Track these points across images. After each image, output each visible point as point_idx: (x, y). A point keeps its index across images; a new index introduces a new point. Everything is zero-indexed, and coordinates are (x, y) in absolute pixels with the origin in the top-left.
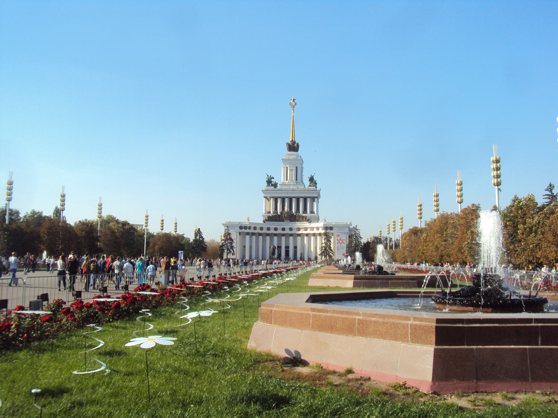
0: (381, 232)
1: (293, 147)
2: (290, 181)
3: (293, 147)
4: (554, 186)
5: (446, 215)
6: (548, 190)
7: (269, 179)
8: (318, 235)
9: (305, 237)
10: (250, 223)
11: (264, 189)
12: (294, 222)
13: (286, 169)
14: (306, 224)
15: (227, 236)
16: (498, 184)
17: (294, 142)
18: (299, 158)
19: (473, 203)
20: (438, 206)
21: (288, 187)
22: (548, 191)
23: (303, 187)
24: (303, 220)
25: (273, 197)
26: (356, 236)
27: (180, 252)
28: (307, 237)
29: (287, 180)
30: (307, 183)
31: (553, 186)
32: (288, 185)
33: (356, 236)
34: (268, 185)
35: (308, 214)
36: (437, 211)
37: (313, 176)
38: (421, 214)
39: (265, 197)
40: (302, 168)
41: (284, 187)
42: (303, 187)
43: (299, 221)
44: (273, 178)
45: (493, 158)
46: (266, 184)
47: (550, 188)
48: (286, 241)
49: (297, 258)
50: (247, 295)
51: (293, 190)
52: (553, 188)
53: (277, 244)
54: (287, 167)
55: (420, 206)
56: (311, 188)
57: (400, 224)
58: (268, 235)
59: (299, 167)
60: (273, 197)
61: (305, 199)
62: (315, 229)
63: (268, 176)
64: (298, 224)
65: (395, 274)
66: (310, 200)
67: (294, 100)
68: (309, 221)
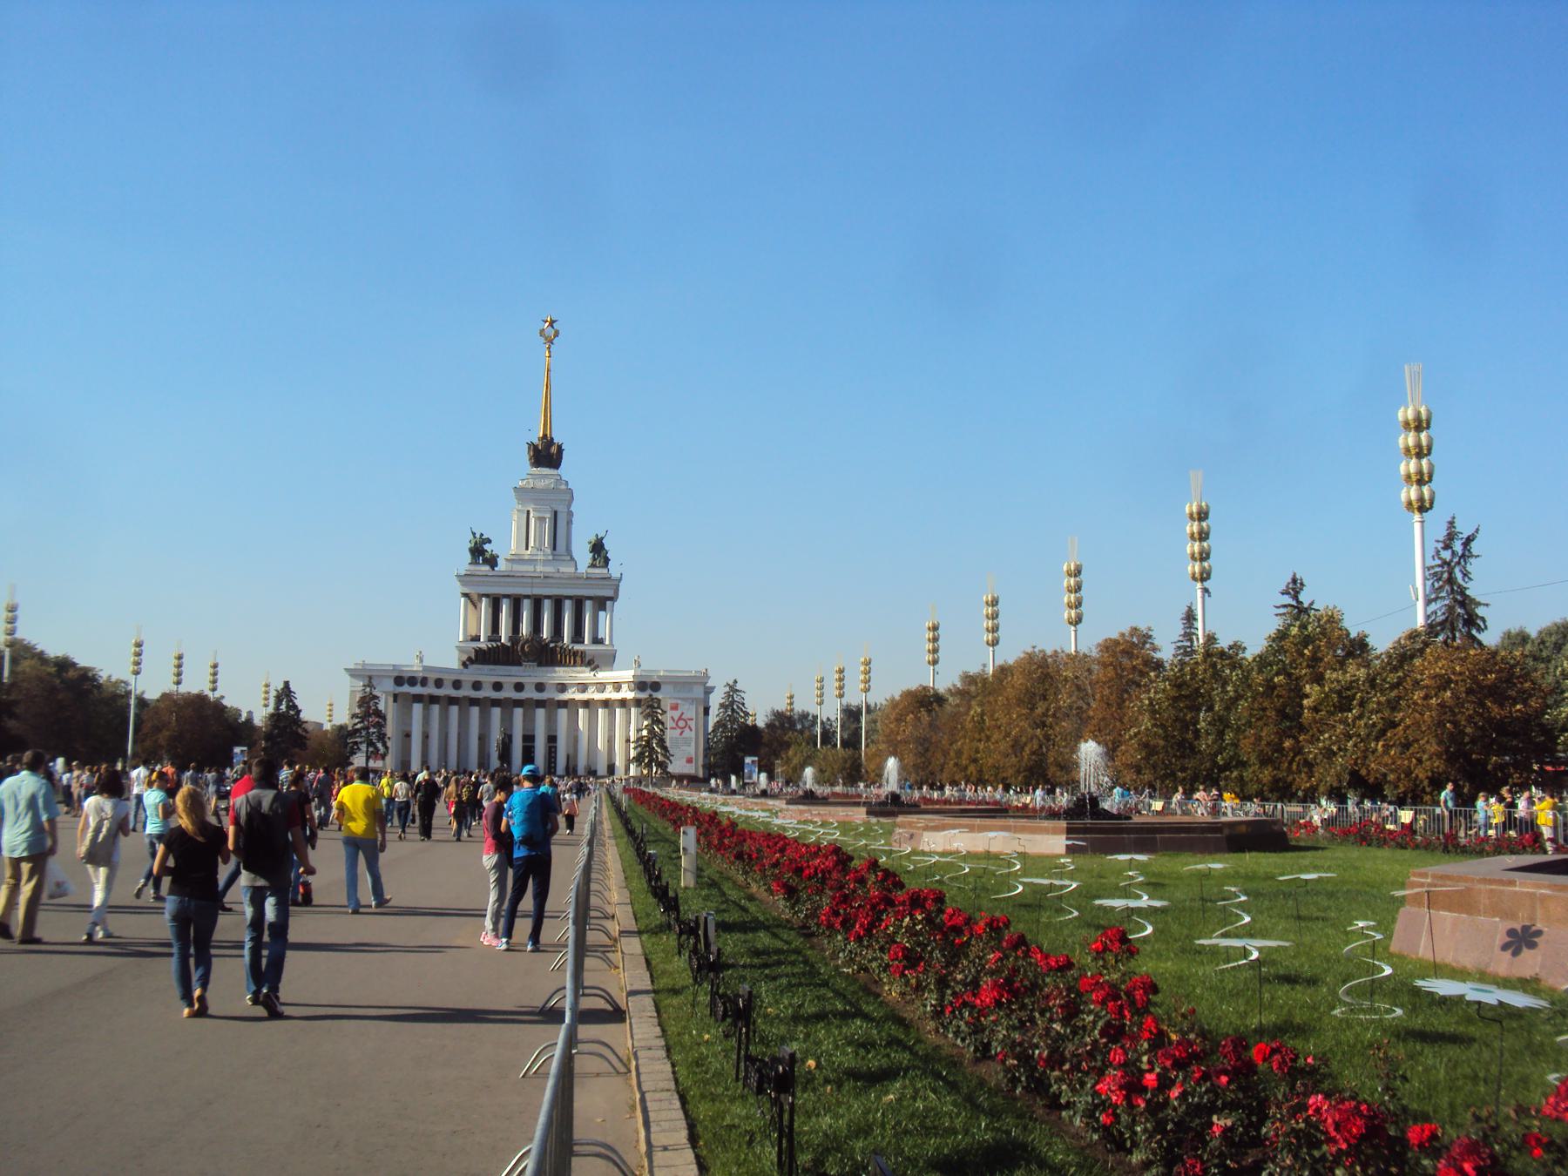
0: (791, 697)
1: (546, 455)
2: (535, 552)
3: (546, 455)
4: (1305, 582)
5: (1041, 655)
6: (1288, 593)
7: (476, 543)
8: (617, 704)
9: (581, 711)
10: (426, 669)
11: (463, 573)
12: (550, 668)
13: (525, 516)
14: (585, 675)
15: (367, 706)
16: (1204, 576)
17: (548, 441)
18: (563, 487)
19: (1134, 626)
20: (997, 629)
21: (530, 568)
22: (1286, 597)
23: (573, 570)
24: (575, 662)
25: (487, 596)
26: (733, 710)
27: (748, 760)
28: (587, 710)
29: (527, 549)
30: (583, 556)
31: (1302, 584)
32: (531, 561)
33: (733, 710)
34: (474, 562)
35: (587, 645)
36: (993, 645)
37: (602, 538)
38: (935, 651)
39: (466, 595)
40: (570, 514)
41: (518, 568)
42: (573, 570)
43: (564, 666)
44: (489, 541)
45: (1191, 506)
46: (468, 558)
47: (1293, 589)
48: (503, 720)
49: (555, 767)
50: (1424, 889)
51: (545, 577)
52: (1302, 589)
53: (524, 729)
54: (528, 511)
55: (935, 628)
56: (597, 571)
57: (862, 677)
58: (474, 702)
59: (562, 509)
60: (487, 596)
61: (579, 603)
62: (609, 688)
63: (474, 534)
64: (562, 674)
65: (1130, 818)
66: (594, 605)
67: (552, 323)
68: (592, 663)
